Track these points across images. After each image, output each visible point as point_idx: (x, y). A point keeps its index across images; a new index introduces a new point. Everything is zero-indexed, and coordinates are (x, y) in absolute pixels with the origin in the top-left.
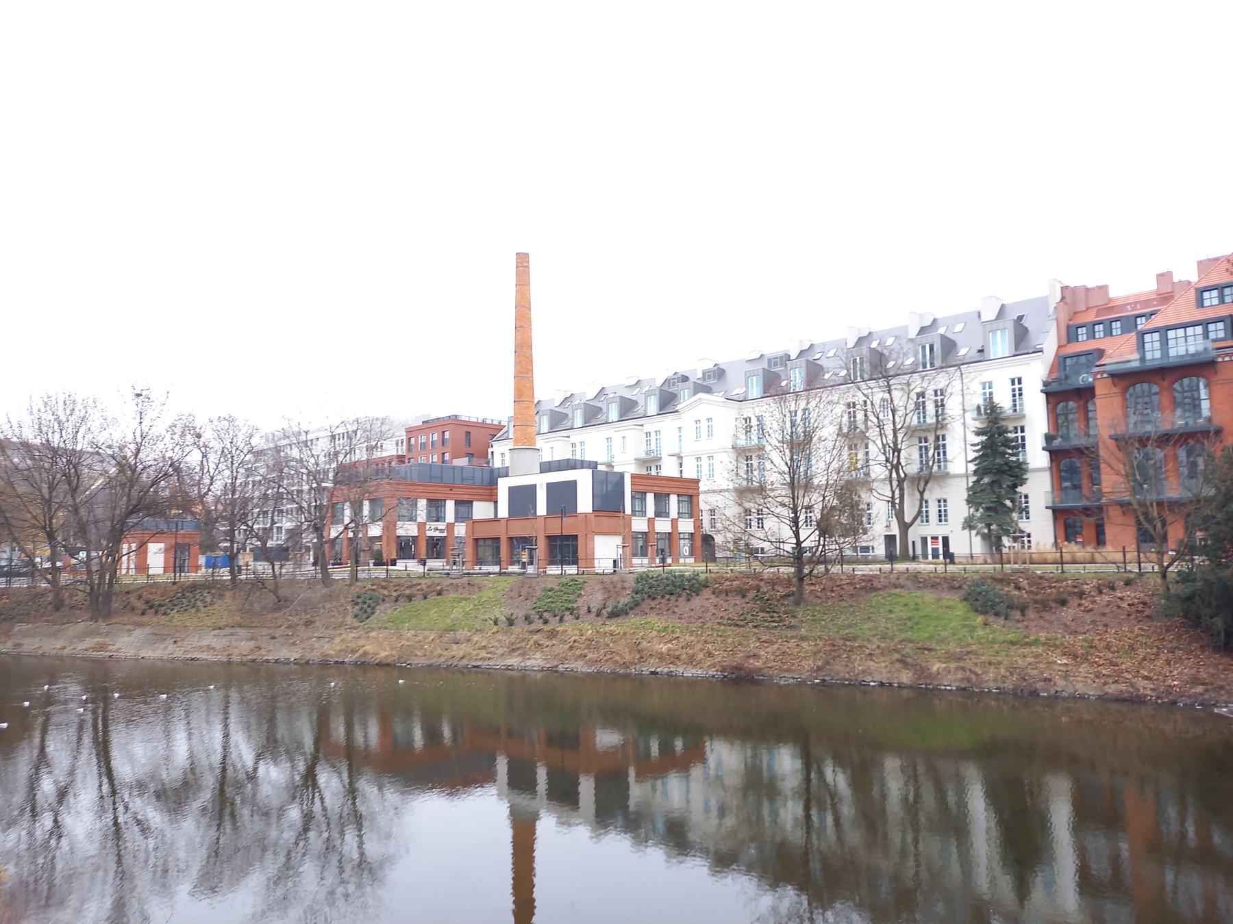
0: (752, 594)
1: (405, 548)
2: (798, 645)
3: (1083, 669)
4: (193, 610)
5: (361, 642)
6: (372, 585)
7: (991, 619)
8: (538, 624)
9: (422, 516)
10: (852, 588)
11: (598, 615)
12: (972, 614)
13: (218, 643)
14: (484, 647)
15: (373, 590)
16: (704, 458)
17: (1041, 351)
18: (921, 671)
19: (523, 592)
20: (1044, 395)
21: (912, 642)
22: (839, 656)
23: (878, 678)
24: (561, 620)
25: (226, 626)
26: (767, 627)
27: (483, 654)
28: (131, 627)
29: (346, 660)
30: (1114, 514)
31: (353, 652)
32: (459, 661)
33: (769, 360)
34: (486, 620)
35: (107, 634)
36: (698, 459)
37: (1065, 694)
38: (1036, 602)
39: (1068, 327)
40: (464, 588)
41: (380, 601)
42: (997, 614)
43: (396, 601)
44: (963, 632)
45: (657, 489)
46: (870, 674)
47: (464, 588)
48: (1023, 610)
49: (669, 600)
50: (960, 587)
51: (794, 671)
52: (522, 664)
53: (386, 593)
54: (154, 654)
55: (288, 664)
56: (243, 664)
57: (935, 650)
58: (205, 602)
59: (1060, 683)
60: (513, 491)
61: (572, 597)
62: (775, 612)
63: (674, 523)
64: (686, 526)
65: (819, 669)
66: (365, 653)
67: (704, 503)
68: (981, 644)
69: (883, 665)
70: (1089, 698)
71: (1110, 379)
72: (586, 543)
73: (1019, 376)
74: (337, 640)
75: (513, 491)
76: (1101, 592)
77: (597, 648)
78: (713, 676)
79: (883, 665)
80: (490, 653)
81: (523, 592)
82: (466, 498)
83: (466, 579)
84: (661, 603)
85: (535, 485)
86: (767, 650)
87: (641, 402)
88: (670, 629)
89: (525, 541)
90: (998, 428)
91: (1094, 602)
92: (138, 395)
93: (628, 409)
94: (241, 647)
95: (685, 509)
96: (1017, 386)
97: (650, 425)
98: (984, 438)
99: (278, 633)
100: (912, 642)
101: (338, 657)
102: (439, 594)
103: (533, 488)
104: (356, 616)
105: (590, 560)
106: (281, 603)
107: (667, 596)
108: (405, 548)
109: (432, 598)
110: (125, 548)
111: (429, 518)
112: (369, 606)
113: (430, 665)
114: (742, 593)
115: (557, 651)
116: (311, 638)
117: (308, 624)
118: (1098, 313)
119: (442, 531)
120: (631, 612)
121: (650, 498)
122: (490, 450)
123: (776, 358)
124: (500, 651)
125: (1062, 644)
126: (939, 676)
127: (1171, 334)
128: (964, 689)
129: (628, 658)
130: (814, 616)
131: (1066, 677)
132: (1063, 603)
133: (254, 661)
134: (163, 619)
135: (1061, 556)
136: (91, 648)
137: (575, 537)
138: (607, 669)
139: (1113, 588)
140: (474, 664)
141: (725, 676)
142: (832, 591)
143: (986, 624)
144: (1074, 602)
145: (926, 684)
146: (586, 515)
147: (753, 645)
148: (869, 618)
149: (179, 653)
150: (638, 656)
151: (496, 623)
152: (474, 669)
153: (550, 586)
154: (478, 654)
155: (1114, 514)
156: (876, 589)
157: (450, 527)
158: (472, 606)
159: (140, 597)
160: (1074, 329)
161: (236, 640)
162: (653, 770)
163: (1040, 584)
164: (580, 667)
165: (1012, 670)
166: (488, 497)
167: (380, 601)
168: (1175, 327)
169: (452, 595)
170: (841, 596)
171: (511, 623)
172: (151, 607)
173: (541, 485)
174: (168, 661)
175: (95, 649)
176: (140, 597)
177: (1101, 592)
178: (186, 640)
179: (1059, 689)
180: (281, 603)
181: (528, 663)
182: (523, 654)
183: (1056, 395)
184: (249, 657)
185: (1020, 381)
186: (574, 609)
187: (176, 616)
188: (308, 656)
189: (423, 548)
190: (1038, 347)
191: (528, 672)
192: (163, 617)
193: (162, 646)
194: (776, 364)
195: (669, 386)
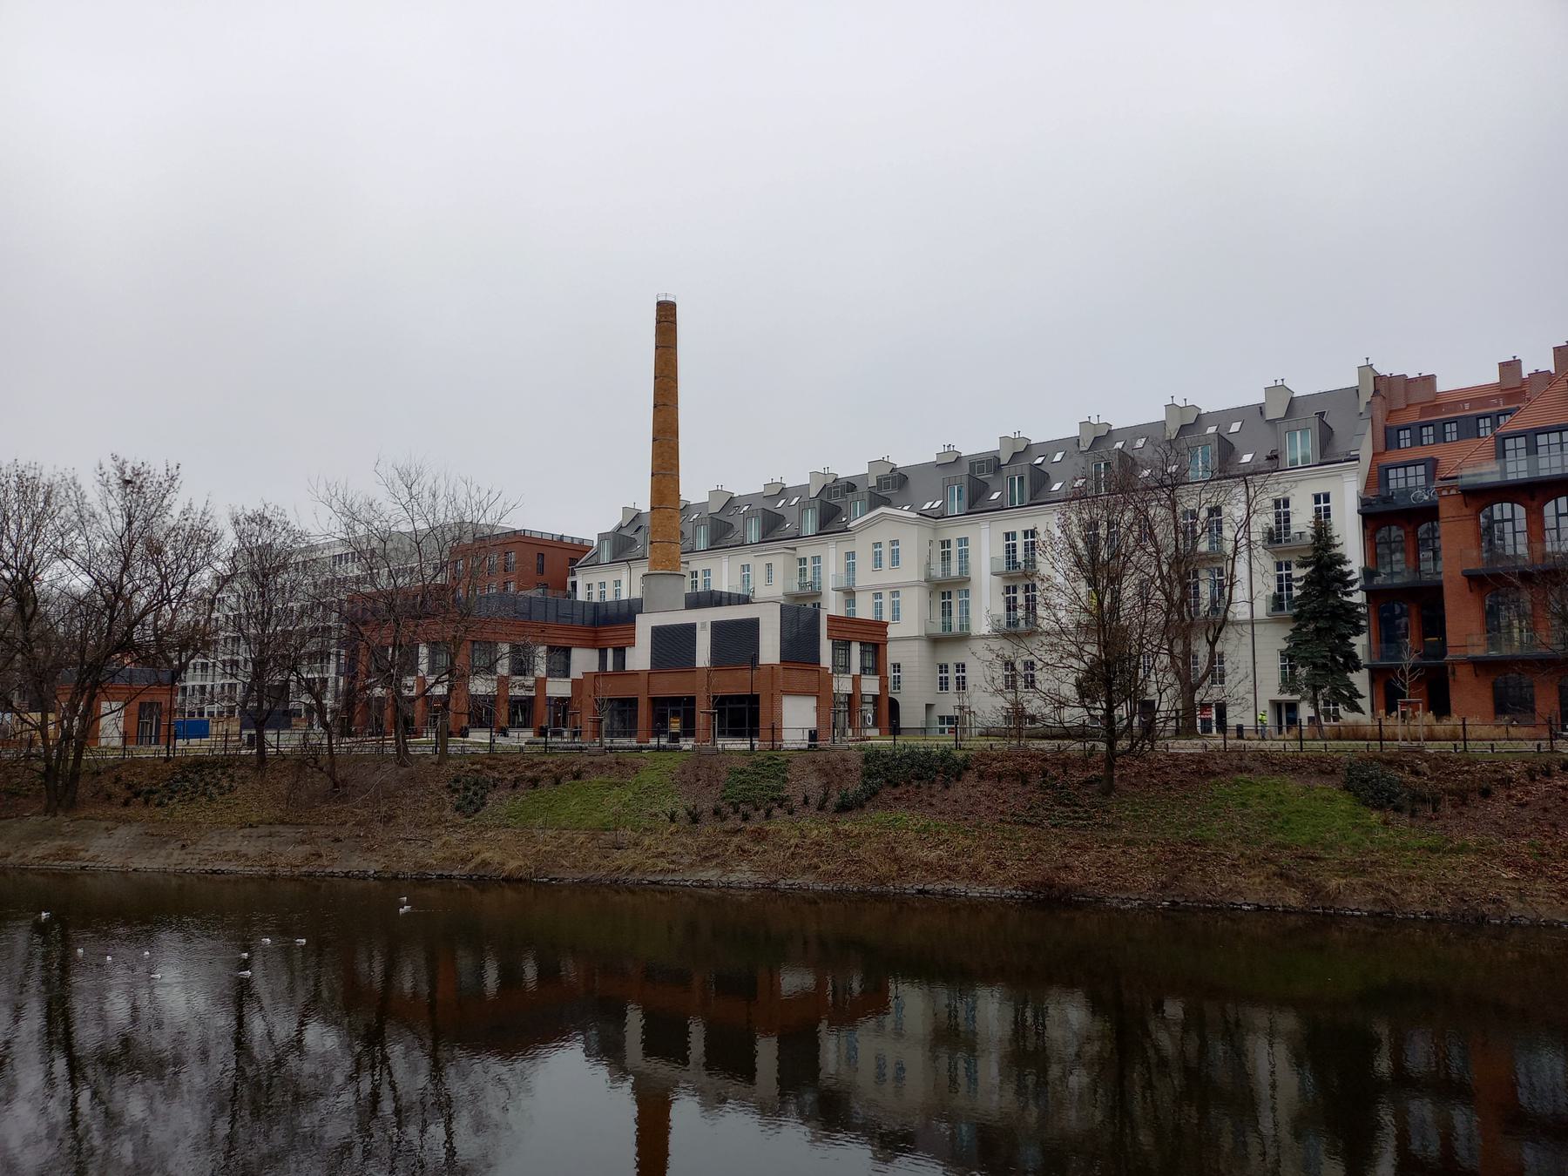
0: (1036, 780)
1: (482, 713)
2: (1124, 852)
3: (1541, 885)
4: (204, 799)
5: (475, 847)
6: (473, 764)
7: (1392, 816)
8: (734, 822)
9: (503, 668)
10: (1179, 772)
11: (821, 808)
12: (1360, 809)
13: (251, 848)
14: (662, 855)
15: (476, 771)
16: (886, 595)
17: (1357, 459)
18: (1316, 891)
19: (703, 774)
20: (1361, 516)
21: (1286, 847)
22: (1189, 868)
23: (1252, 899)
24: (768, 815)
25: (261, 822)
26: (1072, 826)
27: (663, 863)
28: (109, 824)
29: (455, 873)
30: (1464, 674)
31: (464, 861)
32: (627, 874)
33: (972, 465)
34: (656, 815)
35: (74, 835)
36: (878, 595)
37: (1524, 921)
38: (1450, 792)
39: (1386, 429)
40: (611, 768)
41: (491, 788)
42: (1398, 809)
43: (514, 787)
44: (1356, 835)
45: (867, 638)
46: (1240, 893)
47: (611, 768)
48: (1435, 802)
49: (918, 787)
50: (1333, 771)
51: (1127, 889)
52: (724, 879)
53: (496, 775)
54: (155, 862)
55: (364, 879)
56: (292, 879)
57: (1325, 859)
58: (221, 787)
59: (1516, 907)
60: (658, 633)
61: (774, 782)
62: (1076, 805)
63: (856, 681)
64: (871, 686)
65: (1165, 886)
66: (485, 863)
67: (893, 653)
68: (1385, 850)
69: (1257, 880)
70: (1560, 926)
71: (1460, 499)
72: (772, 707)
73: (1325, 491)
74: (436, 844)
75: (658, 633)
76: (1533, 779)
77: (832, 855)
78: (1012, 897)
79: (1257, 880)
80: (673, 862)
81: (703, 774)
82: (562, 642)
83: (611, 756)
84: (908, 791)
85: (695, 625)
86: (1081, 859)
87: (738, 526)
88: (934, 829)
89: (684, 707)
90: (1329, 557)
91: (1528, 793)
92: (128, 482)
93: (773, 526)
94: (289, 854)
95: (869, 663)
96: (1282, 509)
97: (807, 551)
98: (1309, 569)
99: (343, 833)
100: (1286, 847)
101: (443, 869)
102: (577, 776)
103: (690, 630)
104: (458, 809)
105: (775, 731)
106: (339, 790)
107: (915, 783)
108: (482, 713)
109: (567, 782)
110: (105, 706)
111: (551, 673)
112: (475, 794)
113: (586, 881)
114: (1023, 778)
115: (773, 861)
116: (394, 841)
117: (388, 819)
118: (1424, 412)
119: (529, 688)
120: (868, 805)
121: (856, 649)
122: (570, 580)
123: (983, 462)
124: (686, 860)
125: (1501, 850)
126: (1341, 897)
127: (1542, 439)
128: (1380, 915)
129: (884, 870)
130: (1136, 811)
131: (1521, 896)
132: (1486, 793)
133: (310, 875)
134: (160, 813)
135: (1380, 729)
136: (50, 855)
137: (754, 699)
138: (852, 885)
139: (1548, 773)
140: (652, 878)
141: (1029, 897)
142: (1152, 776)
143: (1386, 823)
144: (1501, 793)
145: (1324, 908)
146: (772, 666)
147: (1056, 850)
148: (1215, 814)
149: (191, 863)
150: (896, 867)
151: (672, 819)
152: (652, 886)
153: (740, 767)
154: (654, 865)
155: (1464, 674)
156: (1214, 774)
157: (540, 684)
158: (630, 795)
159: (118, 780)
160: (1396, 432)
161: (279, 844)
162: (847, 1015)
163: (1447, 767)
164: (808, 881)
165: (1443, 888)
166: (591, 643)
167: (491, 788)
168: (1547, 431)
169: (596, 779)
170: (1167, 783)
171: (695, 818)
172: (137, 795)
173: (704, 624)
174: (175, 874)
175: (56, 856)
176: (118, 780)
177: (1533, 779)
178: (201, 842)
179: (1516, 914)
180: (339, 790)
181: (733, 878)
182: (723, 865)
183: (1374, 517)
184: (304, 869)
185: (1327, 498)
186: (784, 799)
187: (179, 807)
188: (396, 867)
189: (503, 715)
190: (1352, 453)
191: (732, 891)
192: (158, 809)
193: (163, 853)
194: (981, 471)
195: (829, 497)
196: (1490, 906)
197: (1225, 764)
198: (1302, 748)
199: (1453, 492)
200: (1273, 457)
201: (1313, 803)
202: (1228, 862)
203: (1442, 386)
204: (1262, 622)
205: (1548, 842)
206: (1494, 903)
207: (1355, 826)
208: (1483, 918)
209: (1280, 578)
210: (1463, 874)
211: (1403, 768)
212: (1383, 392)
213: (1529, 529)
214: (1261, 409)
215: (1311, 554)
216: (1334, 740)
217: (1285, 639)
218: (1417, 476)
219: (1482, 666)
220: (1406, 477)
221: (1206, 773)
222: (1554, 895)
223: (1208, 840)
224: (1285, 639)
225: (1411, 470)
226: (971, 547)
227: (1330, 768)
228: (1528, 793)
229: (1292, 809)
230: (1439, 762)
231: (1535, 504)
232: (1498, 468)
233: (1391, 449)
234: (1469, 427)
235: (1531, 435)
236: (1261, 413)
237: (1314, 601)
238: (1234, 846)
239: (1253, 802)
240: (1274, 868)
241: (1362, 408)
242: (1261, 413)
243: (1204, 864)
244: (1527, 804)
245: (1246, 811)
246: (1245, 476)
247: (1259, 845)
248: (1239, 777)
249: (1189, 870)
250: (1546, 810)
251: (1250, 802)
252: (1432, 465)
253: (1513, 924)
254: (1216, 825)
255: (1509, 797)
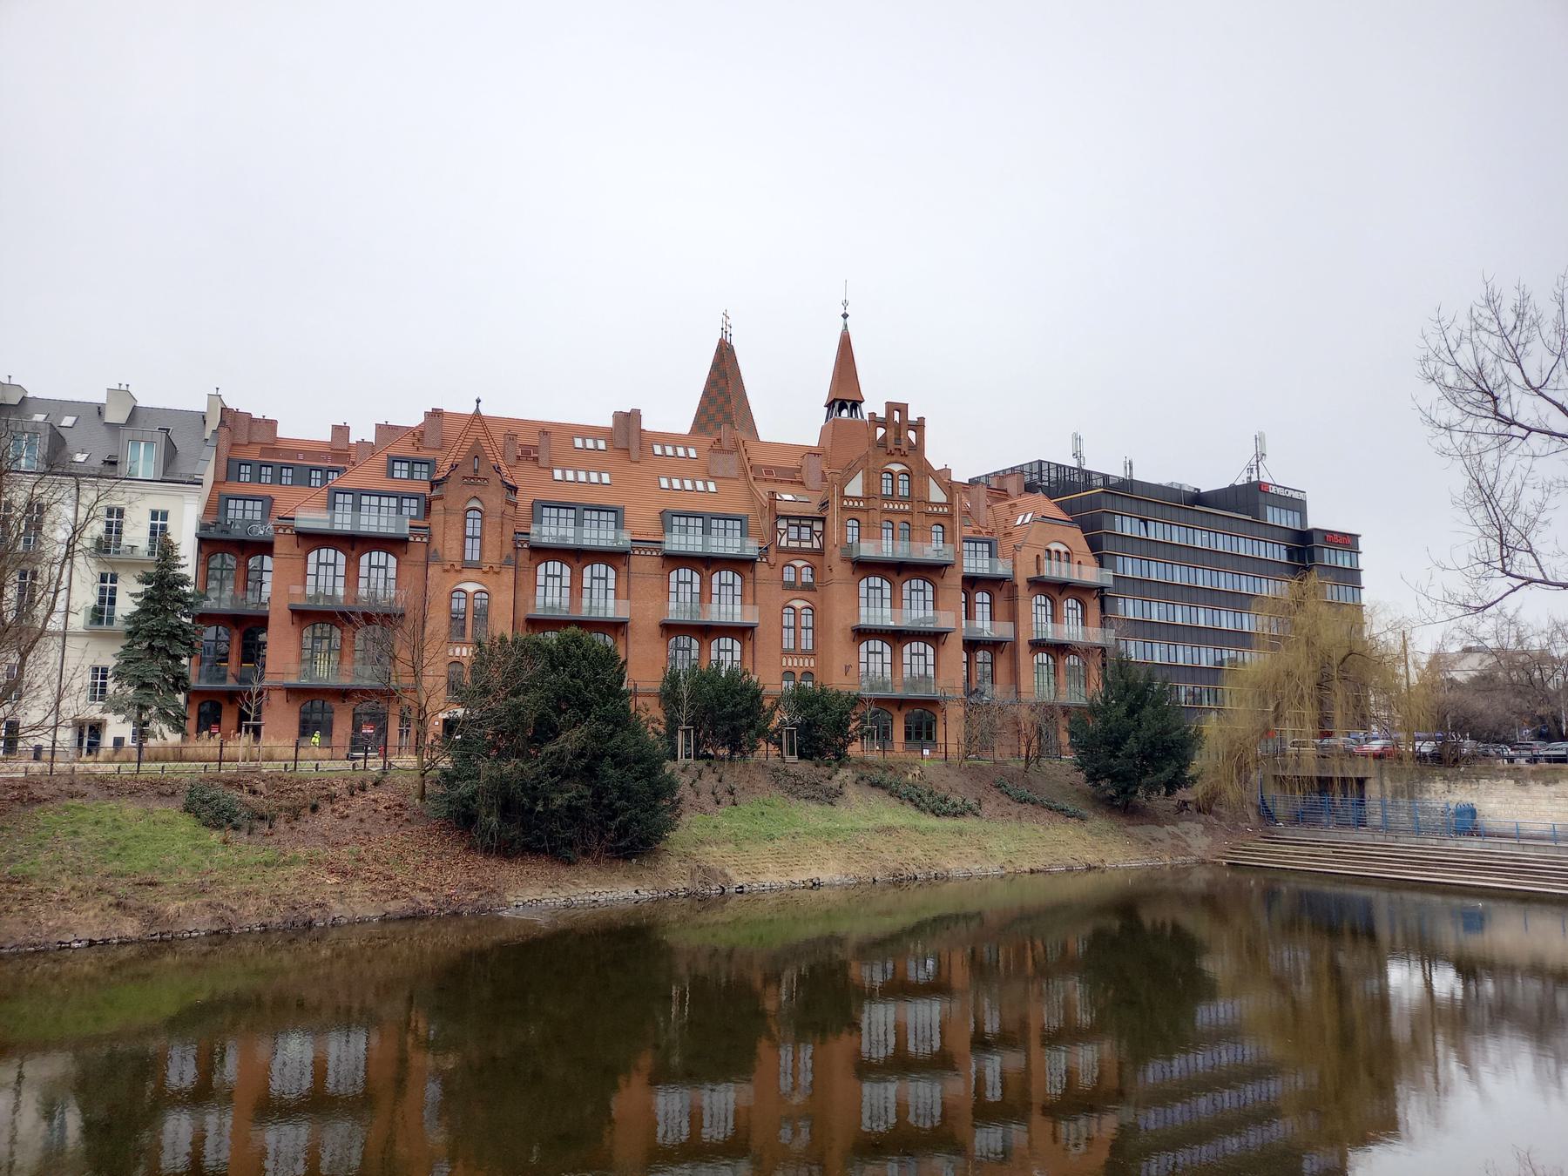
3: (357, 887)
7: (231, 834)
12: (203, 830)
18: (154, 917)
30: (277, 699)
42: (236, 828)
44: (196, 856)
46: (70, 930)
59: (337, 909)
69: (91, 913)
76: (352, 794)
79: (91, 913)
118: (264, 451)
127: (365, 500)
128: (217, 933)
143: (225, 842)
144: (326, 807)
156: (39, 801)
183: (209, 544)
185: (165, 516)
190: (196, 477)
196: (316, 910)
197: (52, 789)
198: (138, 771)
199: (288, 531)
200: (112, 463)
201: (152, 827)
202: (56, 897)
203: (282, 433)
204: (76, 635)
205: (363, 848)
206: (320, 907)
207: (195, 847)
208: (310, 923)
209: (103, 590)
210: (293, 883)
211: (242, 787)
212: (228, 423)
213: (346, 576)
214: (100, 410)
215: (154, 570)
216: (175, 761)
217: (114, 656)
218: (254, 511)
219: (294, 692)
220: (244, 510)
221: (29, 800)
222: (367, 894)
223: (33, 875)
224: (114, 656)
225: (249, 504)
226: (171, 524)
227: (170, 791)
228: (347, 807)
229: (129, 835)
230: (275, 782)
231: (354, 554)
232: (328, 517)
233: (232, 480)
234: (302, 476)
235: (358, 494)
236: (100, 413)
237: (152, 619)
238: (64, 879)
239: (86, 829)
240: (110, 899)
241: (208, 435)
242: (100, 413)
243: (27, 903)
244: (347, 816)
245: (77, 840)
246: (79, 476)
247: (93, 874)
248: (70, 802)
249: (7, 911)
250: (361, 820)
251: (83, 830)
252: (268, 502)
253: (335, 924)
254: (42, 858)
255: (333, 811)
